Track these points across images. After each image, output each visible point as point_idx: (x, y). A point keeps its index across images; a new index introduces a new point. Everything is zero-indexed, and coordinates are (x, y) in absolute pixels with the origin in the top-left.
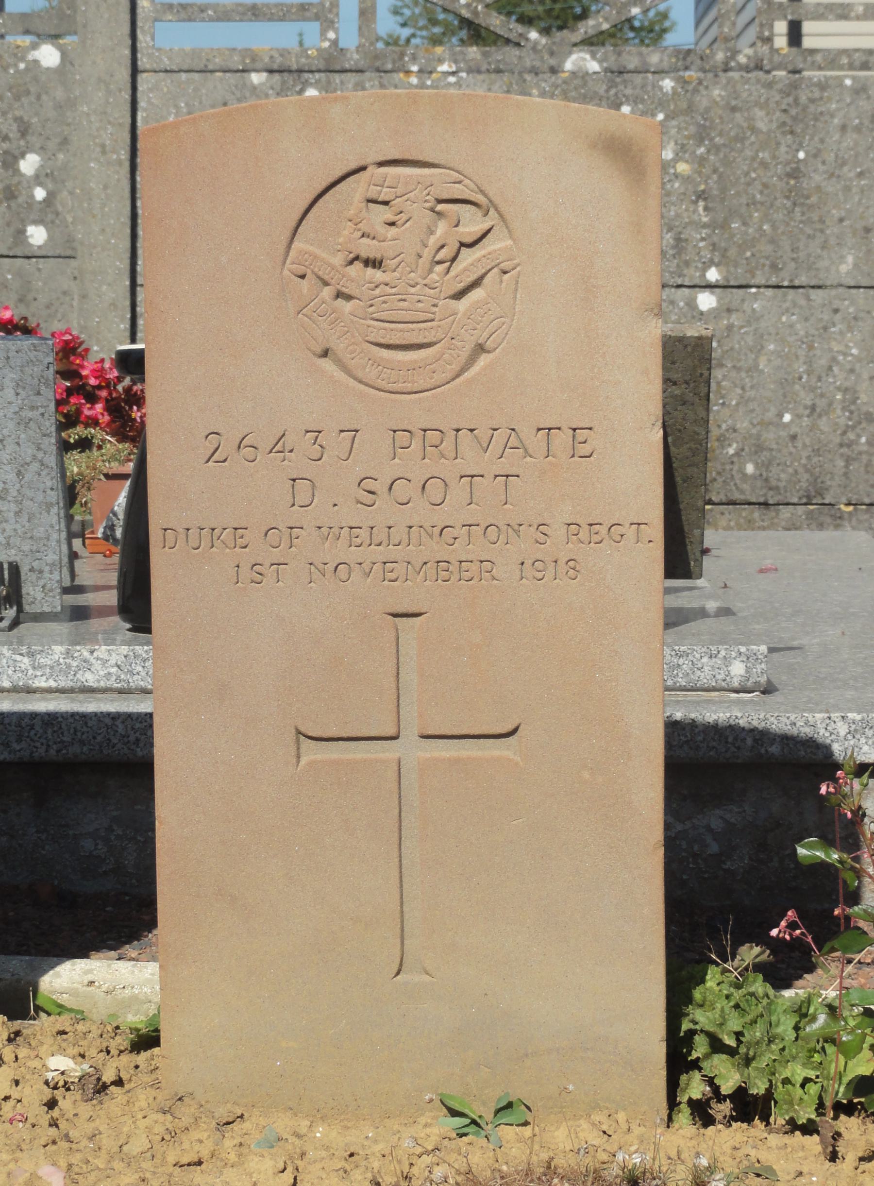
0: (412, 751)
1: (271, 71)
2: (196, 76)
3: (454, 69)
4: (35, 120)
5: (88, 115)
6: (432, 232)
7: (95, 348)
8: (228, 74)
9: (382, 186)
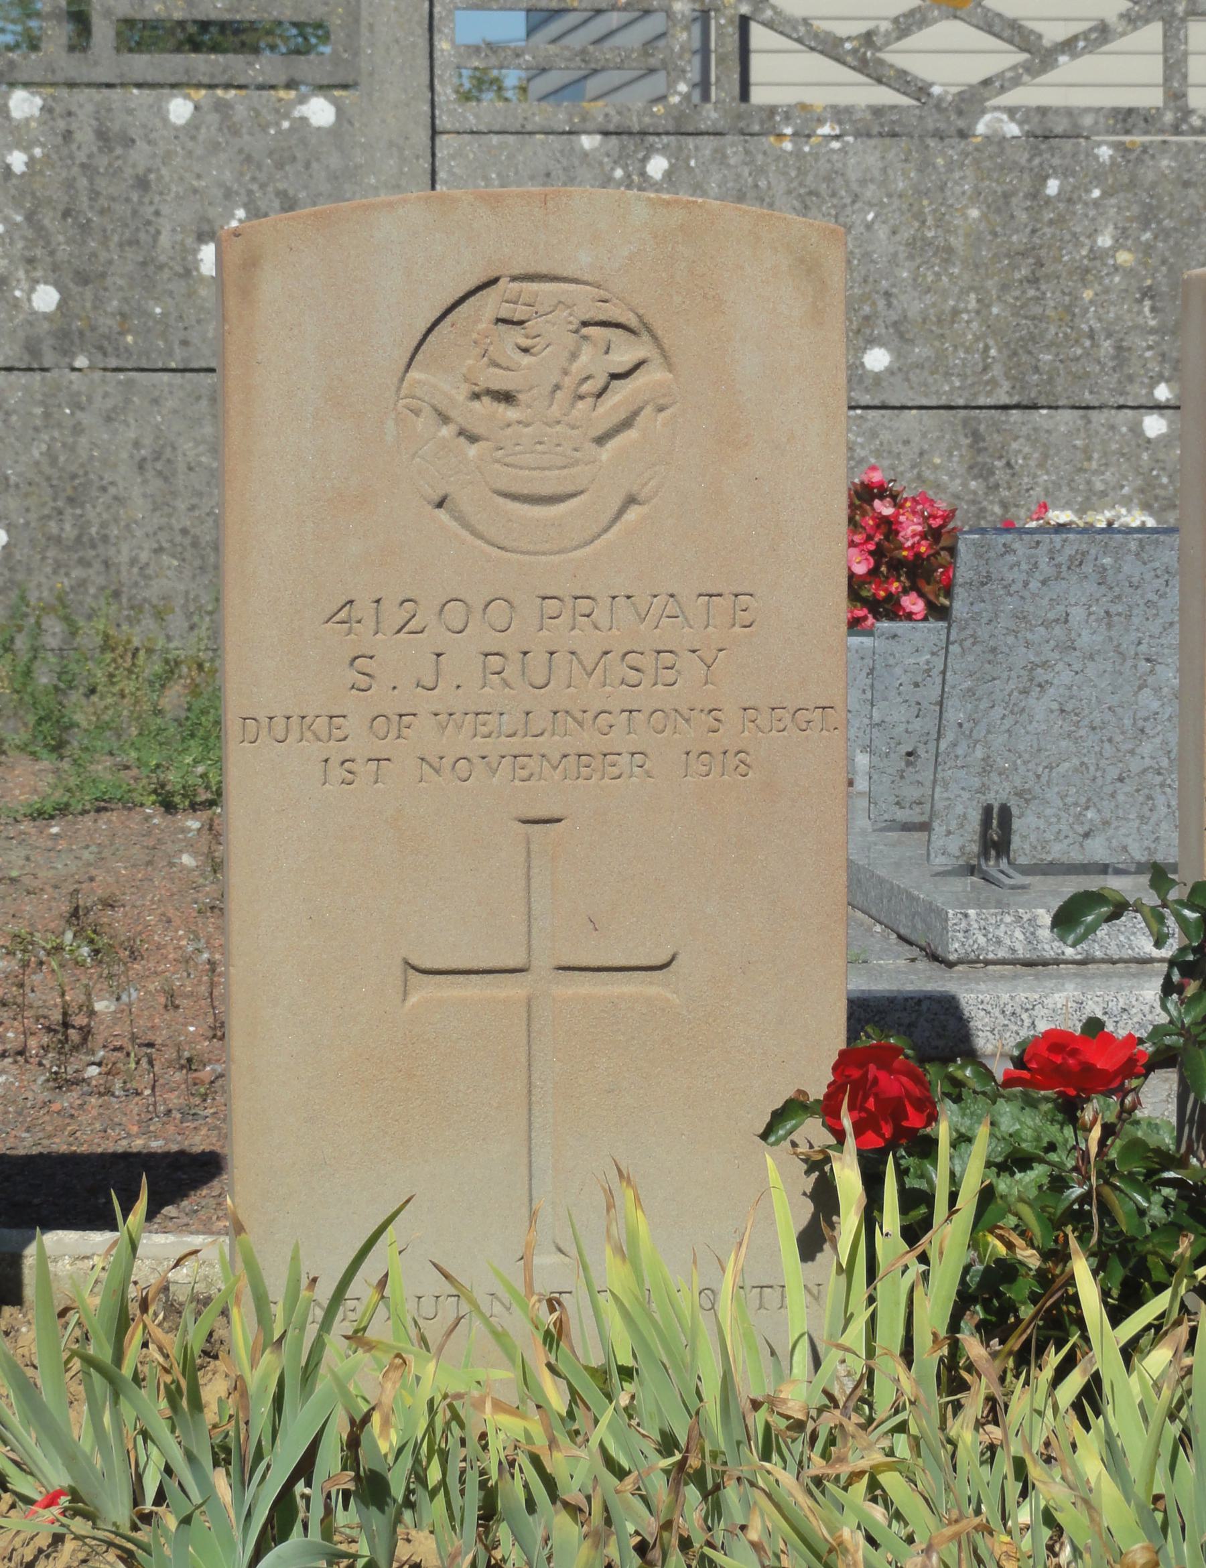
1: (606, 134)
2: (511, 139)
3: (837, 132)
9: (515, 303)
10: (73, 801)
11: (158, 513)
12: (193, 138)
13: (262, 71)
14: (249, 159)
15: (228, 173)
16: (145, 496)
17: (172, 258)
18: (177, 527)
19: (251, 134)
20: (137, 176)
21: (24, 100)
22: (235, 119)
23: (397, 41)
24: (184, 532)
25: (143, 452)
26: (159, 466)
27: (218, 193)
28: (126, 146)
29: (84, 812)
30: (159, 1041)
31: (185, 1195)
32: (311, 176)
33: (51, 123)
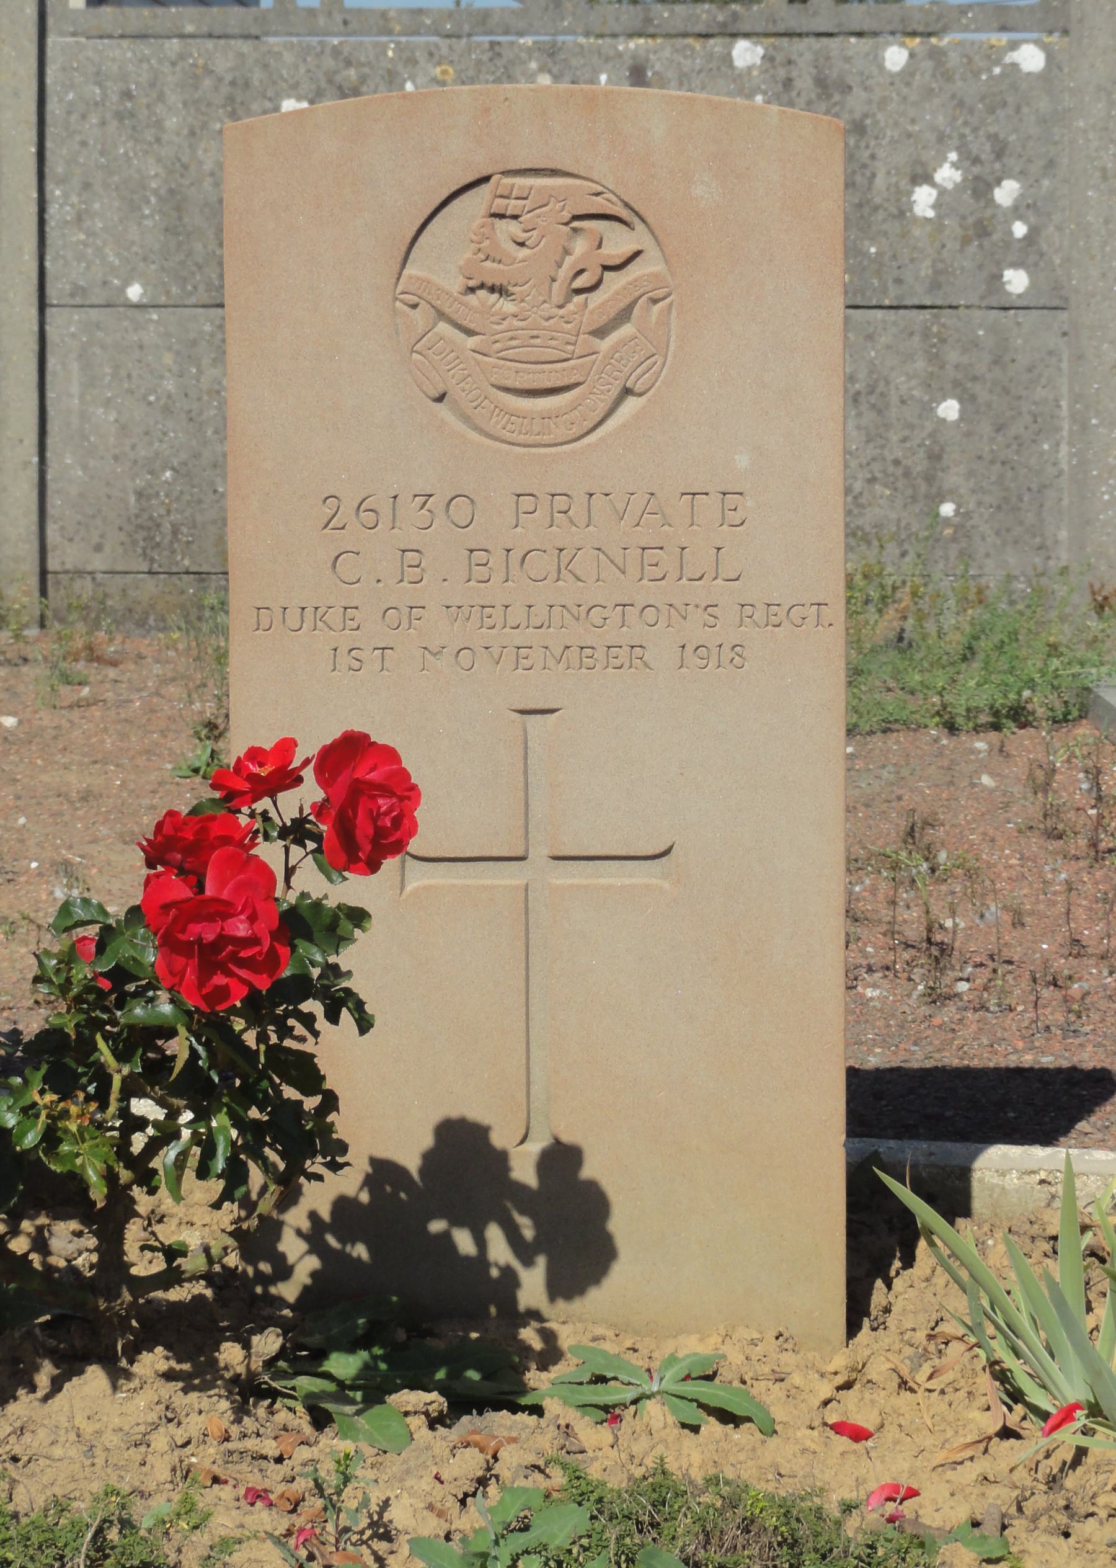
4: (1013, 138)
5: (1085, 131)
6: (567, 252)
9: (507, 197)
10: (861, 723)
11: (871, 445)
12: (908, 84)
14: (961, 104)
15: (941, 118)
16: (859, 428)
17: (888, 200)
18: (890, 458)
19: (965, 80)
20: (854, 121)
21: (746, 50)
22: (949, 65)
24: (897, 462)
25: (857, 386)
26: (873, 399)
27: (931, 137)
28: (843, 92)
29: (872, 733)
30: (1016, 958)
31: (1090, 1112)
32: (1021, 120)
33: (772, 71)
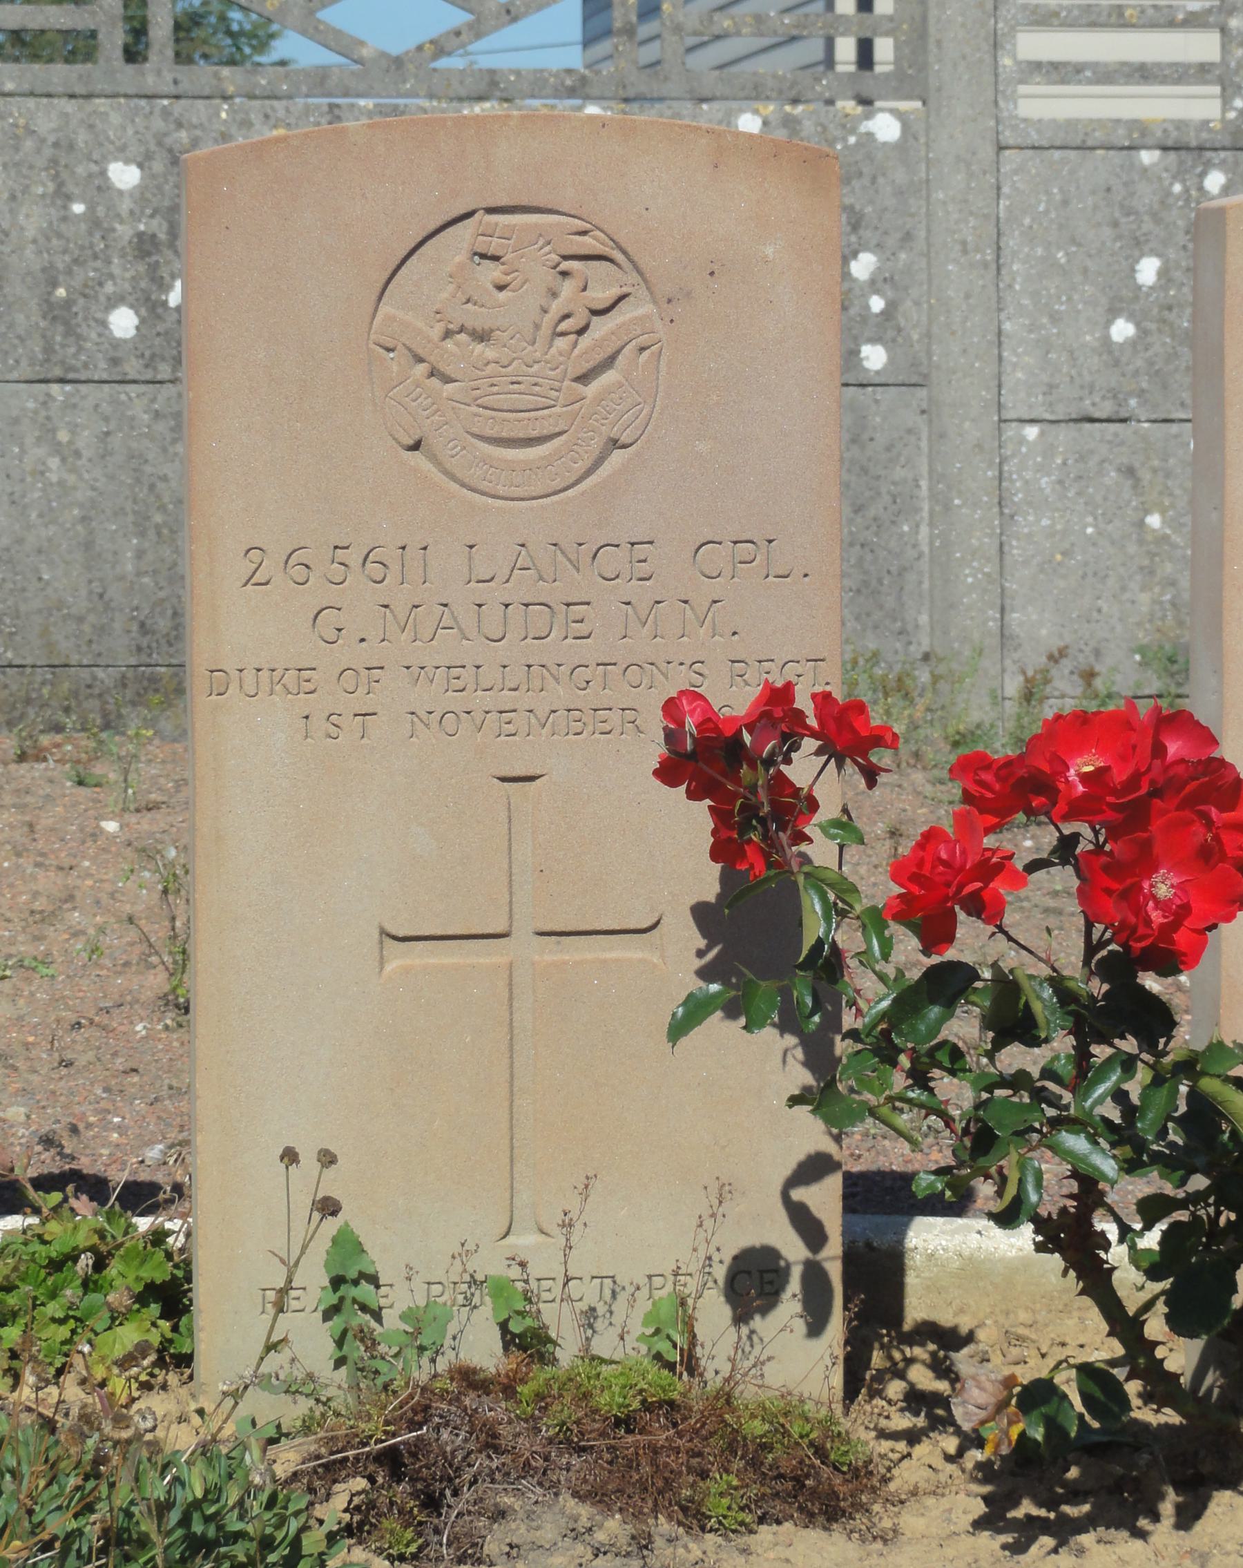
0: (525, 950)
1: (1165, 149)
2: (1072, 154)
4: (869, 209)
5: (944, 203)
6: (554, 295)
7: (957, 502)
8: (1112, 153)
13: (828, 87)
23: (964, 57)
32: (877, 191)
